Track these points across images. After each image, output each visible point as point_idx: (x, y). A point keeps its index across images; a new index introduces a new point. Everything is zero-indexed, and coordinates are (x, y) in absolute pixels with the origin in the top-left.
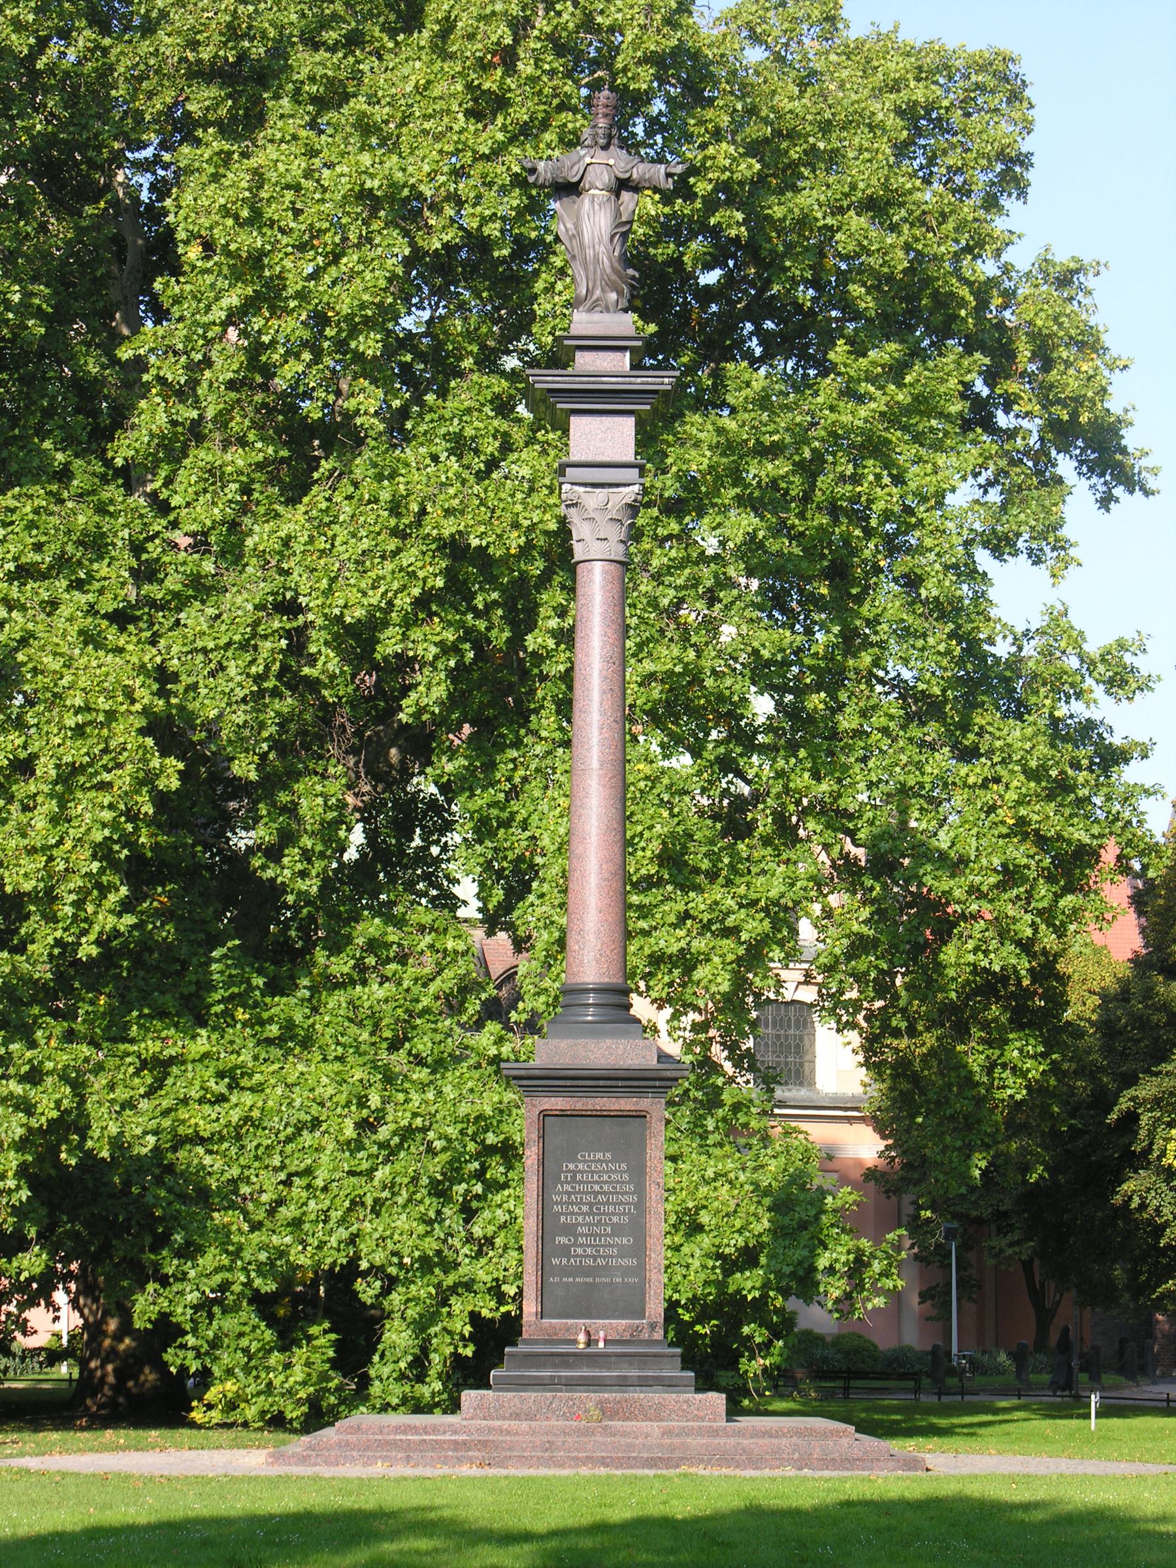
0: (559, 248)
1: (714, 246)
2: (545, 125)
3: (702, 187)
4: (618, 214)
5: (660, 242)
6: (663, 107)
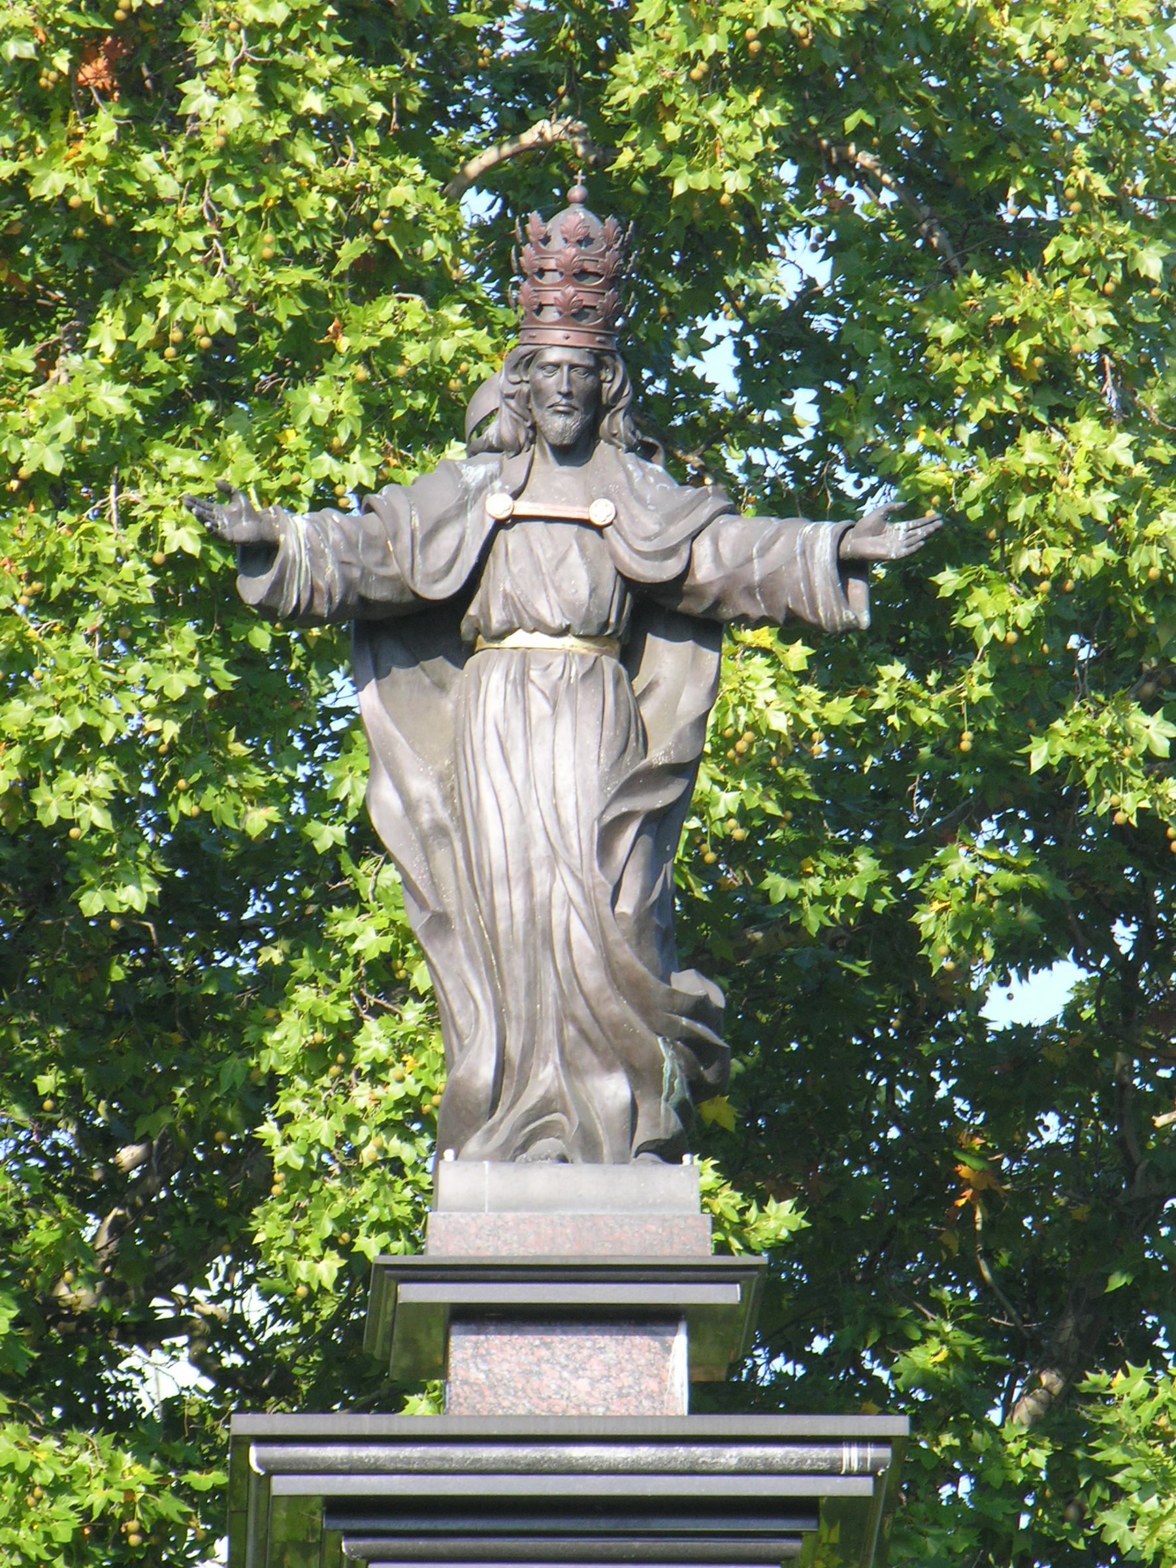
0: (368, 877)
1: (1050, 861)
2: (306, 353)
3: (994, 611)
4: (633, 732)
5: (810, 847)
6: (822, 271)
